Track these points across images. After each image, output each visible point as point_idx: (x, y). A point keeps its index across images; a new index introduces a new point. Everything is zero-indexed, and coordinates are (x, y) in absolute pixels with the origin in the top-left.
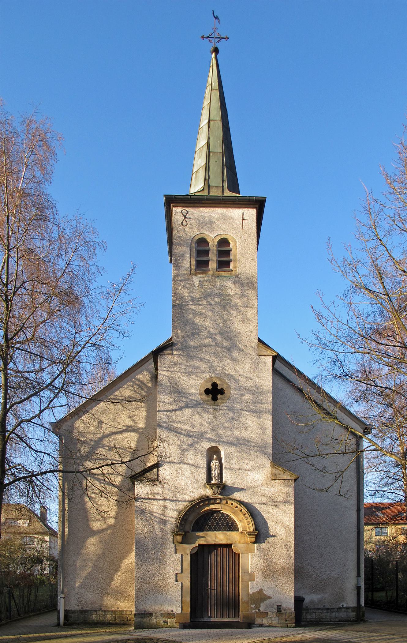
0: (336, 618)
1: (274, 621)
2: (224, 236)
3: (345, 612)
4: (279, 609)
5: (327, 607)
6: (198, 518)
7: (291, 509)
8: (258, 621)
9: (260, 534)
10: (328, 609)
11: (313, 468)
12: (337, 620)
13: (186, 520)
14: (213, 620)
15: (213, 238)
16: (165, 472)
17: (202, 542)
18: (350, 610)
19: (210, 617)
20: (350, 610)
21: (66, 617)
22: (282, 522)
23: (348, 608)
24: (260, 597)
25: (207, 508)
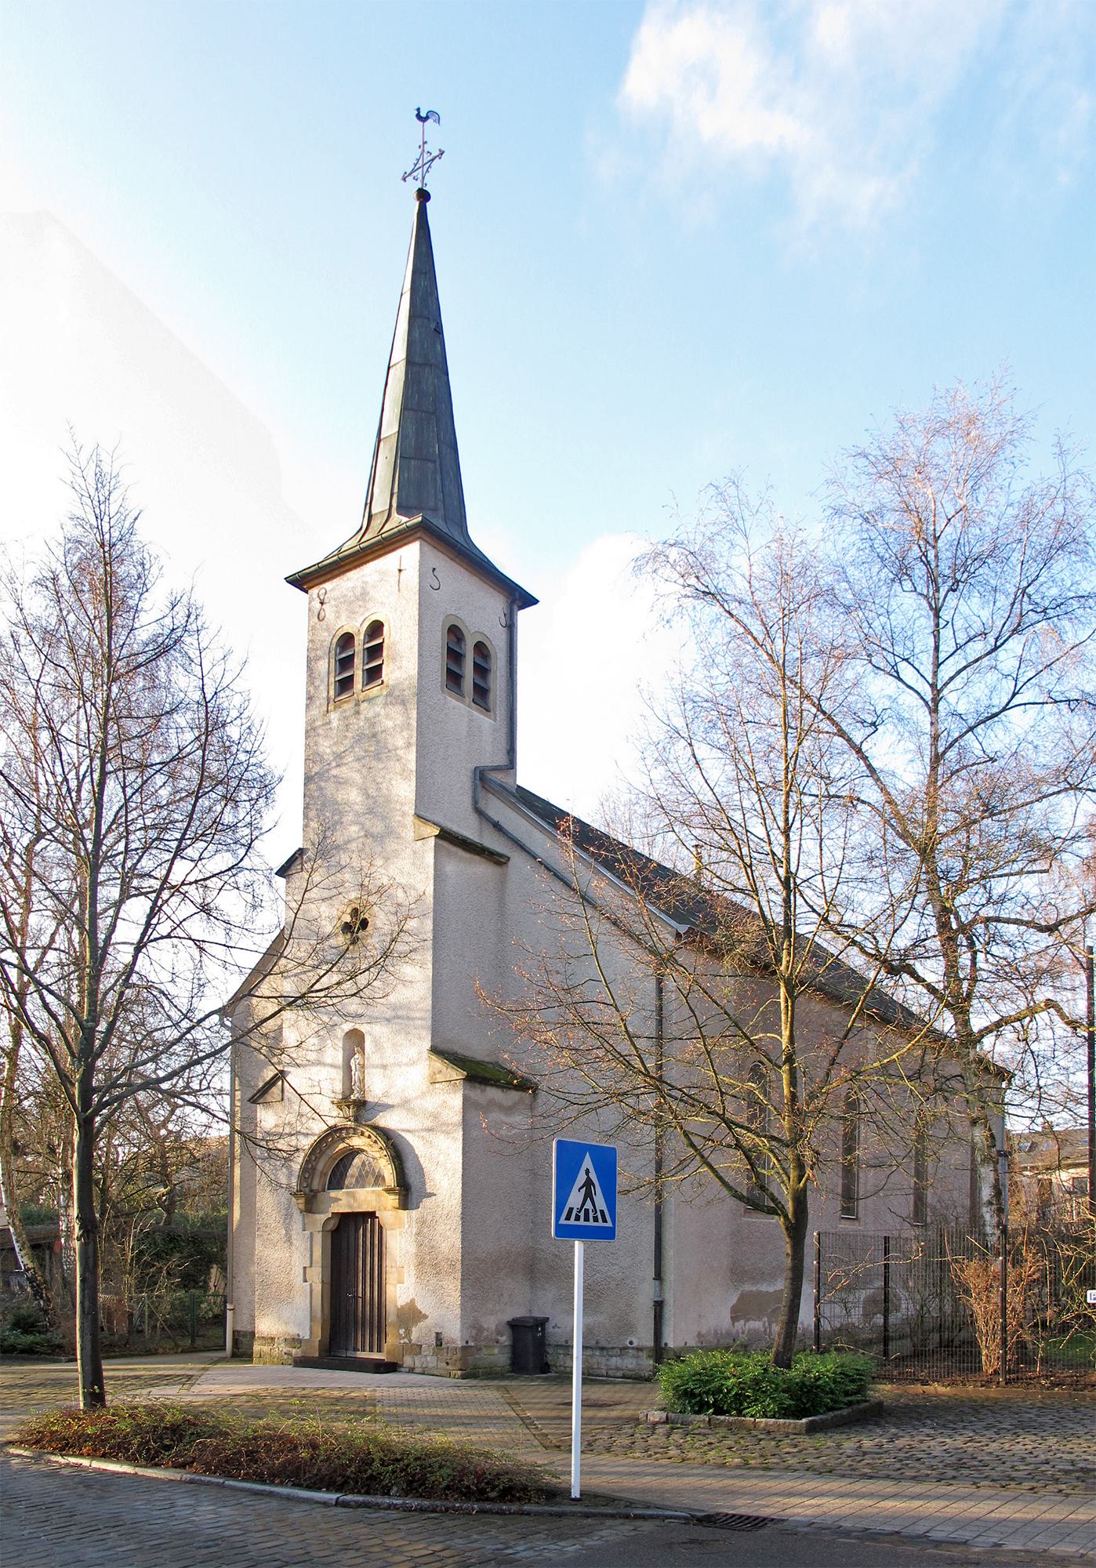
0: (617, 1369)
1: (431, 1361)
2: (374, 618)
3: (634, 1356)
4: (439, 1339)
5: (603, 1344)
6: (330, 1164)
7: (459, 1135)
8: (408, 1361)
9: (408, 1191)
10: (602, 1349)
11: (850, 932)
12: (619, 1374)
13: (314, 1169)
14: (360, 1354)
15: (358, 626)
16: (295, 1078)
17: (342, 1207)
18: (644, 1354)
19: (356, 1350)
20: (644, 1354)
21: (235, 1342)
22: (443, 1163)
23: (639, 1349)
24: (411, 1315)
25: (342, 1146)
